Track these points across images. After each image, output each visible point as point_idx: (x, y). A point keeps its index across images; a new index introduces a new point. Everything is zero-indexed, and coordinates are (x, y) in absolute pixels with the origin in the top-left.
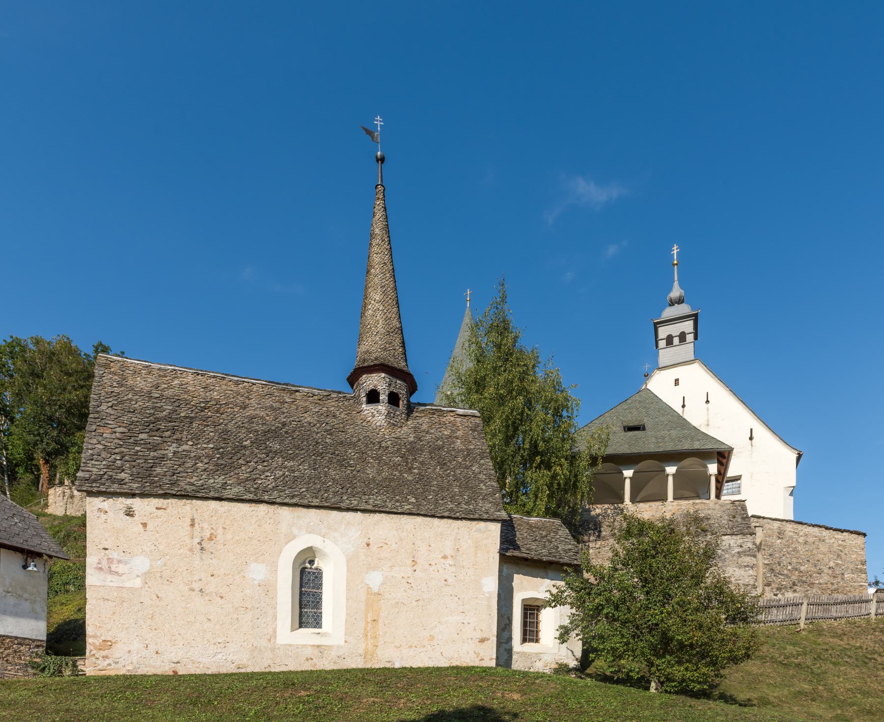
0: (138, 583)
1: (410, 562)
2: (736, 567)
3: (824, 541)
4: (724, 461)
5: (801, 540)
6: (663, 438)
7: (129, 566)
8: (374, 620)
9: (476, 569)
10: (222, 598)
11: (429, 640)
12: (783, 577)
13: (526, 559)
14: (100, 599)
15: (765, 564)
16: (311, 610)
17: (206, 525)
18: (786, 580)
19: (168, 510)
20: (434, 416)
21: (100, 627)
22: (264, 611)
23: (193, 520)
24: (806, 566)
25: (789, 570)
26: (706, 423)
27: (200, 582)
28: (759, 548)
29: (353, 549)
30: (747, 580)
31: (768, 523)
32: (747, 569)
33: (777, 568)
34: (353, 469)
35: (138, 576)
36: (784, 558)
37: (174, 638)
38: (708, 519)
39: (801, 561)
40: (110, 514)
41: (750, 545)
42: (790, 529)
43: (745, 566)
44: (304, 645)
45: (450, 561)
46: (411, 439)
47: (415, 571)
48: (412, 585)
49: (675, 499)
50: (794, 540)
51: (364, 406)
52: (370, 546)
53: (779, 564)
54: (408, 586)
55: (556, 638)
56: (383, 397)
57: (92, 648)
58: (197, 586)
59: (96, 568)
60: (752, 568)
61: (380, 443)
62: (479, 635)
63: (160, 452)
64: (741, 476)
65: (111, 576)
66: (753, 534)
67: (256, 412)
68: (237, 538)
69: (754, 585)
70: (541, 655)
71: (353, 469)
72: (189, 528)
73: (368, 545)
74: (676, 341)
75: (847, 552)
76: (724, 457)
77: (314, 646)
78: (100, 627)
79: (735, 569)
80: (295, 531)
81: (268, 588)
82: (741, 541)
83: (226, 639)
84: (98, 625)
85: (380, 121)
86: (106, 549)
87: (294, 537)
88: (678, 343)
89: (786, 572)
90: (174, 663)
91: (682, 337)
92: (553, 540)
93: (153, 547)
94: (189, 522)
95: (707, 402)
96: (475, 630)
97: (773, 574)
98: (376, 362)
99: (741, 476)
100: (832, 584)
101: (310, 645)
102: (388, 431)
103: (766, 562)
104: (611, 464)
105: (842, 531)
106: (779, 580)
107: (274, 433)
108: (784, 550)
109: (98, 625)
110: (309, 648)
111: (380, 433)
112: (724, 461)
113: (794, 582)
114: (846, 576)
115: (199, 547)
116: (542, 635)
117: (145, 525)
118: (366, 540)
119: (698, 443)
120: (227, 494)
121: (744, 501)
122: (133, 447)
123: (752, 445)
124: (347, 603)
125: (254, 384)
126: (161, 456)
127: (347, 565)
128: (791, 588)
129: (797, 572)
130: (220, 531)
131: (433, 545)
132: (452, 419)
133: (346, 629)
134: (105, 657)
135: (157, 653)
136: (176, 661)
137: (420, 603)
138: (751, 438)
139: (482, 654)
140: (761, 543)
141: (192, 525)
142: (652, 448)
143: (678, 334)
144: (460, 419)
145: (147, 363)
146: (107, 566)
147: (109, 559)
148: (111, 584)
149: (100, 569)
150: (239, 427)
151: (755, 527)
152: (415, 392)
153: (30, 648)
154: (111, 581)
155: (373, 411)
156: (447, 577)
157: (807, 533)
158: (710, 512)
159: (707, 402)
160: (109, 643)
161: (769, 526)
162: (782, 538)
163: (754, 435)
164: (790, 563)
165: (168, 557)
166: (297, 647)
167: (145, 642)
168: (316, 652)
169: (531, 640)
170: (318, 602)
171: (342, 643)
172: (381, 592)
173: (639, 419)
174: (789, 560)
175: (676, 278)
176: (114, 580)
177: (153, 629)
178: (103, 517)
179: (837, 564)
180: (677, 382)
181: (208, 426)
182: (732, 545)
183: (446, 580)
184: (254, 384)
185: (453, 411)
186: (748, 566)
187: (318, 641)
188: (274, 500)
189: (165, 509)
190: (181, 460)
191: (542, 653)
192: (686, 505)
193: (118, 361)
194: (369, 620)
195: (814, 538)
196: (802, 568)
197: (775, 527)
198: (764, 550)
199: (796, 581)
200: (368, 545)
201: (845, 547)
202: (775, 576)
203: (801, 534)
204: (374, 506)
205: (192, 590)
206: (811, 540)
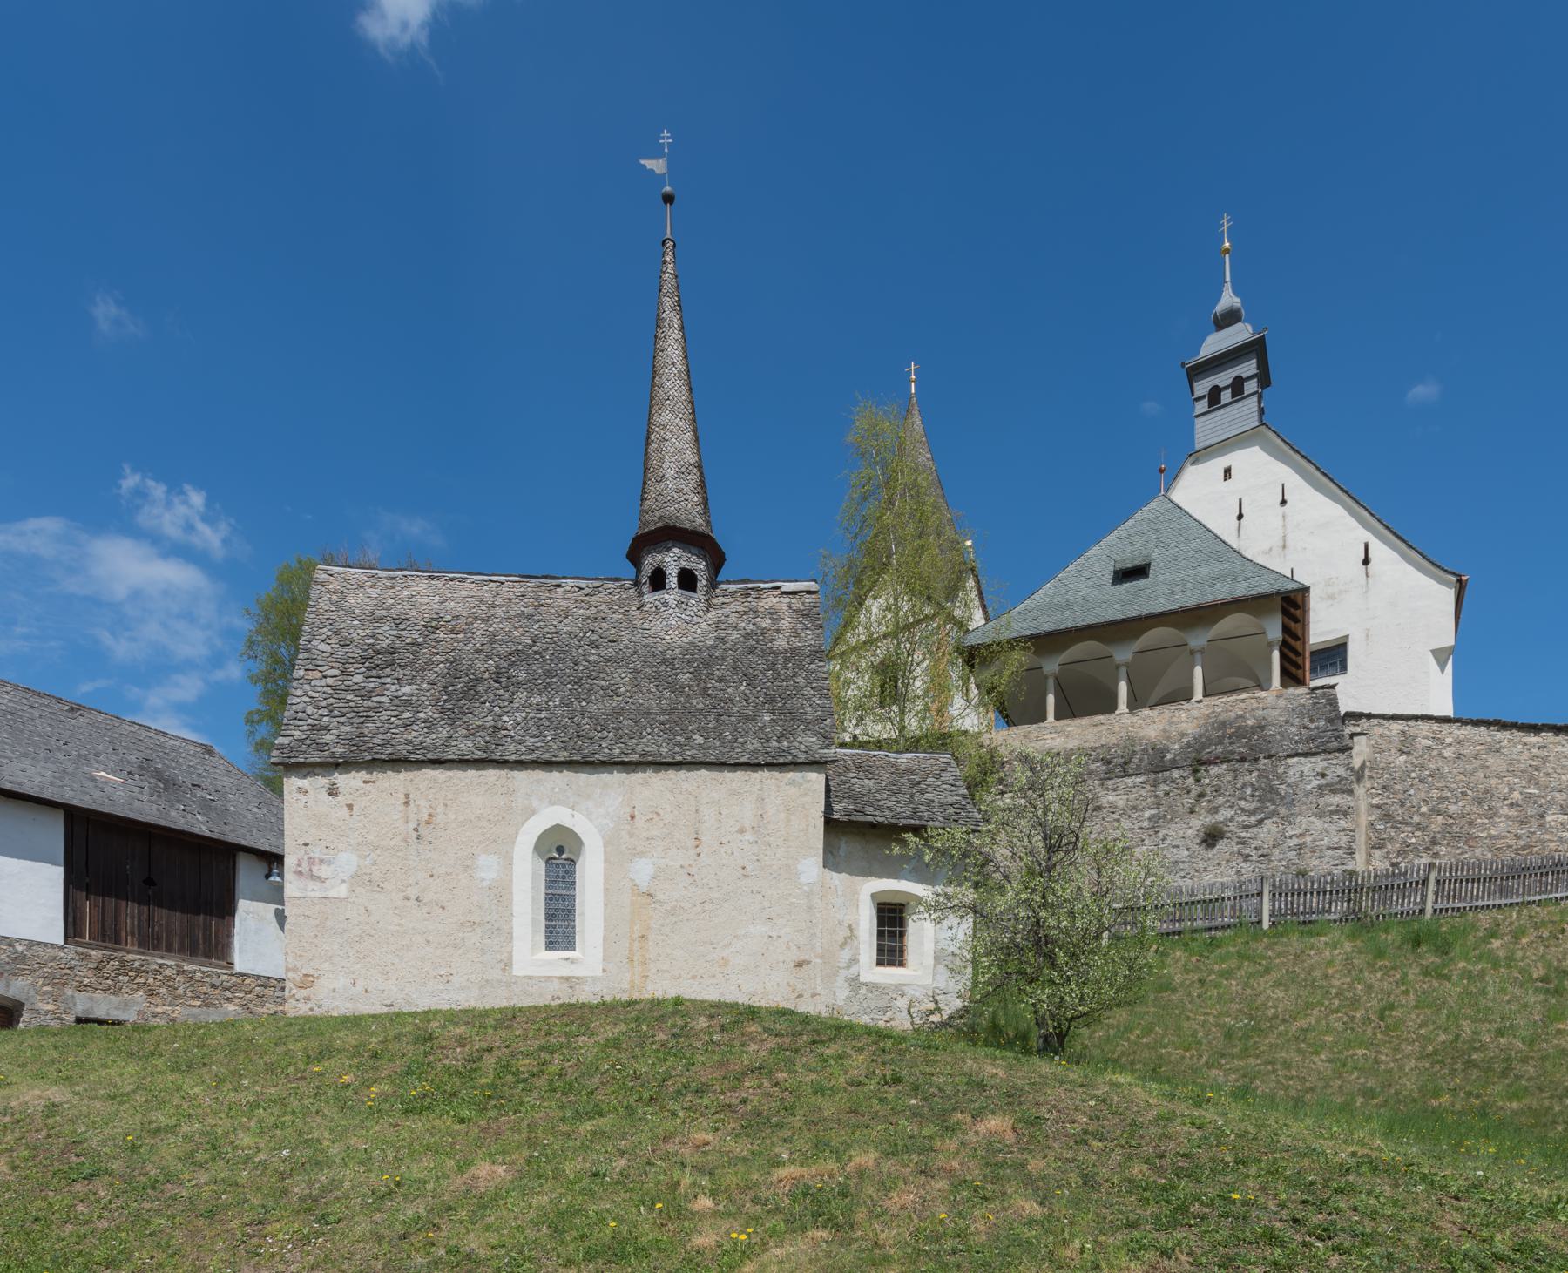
0: (342, 891)
1: (691, 842)
2: (1314, 815)
3: (1498, 751)
4: (1298, 613)
5: (1448, 753)
6: (1184, 583)
7: (333, 867)
8: (643, 937)
9: (789, 847)
10: (443, 908)
11: (720, 966)
12: (1409, 829)
13: (873, 826)
14: (299, 916)
15: (1372, 806)
16: (560, 923)
17: (422, 803)
18: (1417, 834)
19: (378, 784)
20: (749, 599)
21: (300, 956)
22: (496, 926)
23: (407, 796)
24: (1460, 804)
25: (1423, 814)
26: (1281, 543)
27: (417, 887)
28: (1359, 775)
29: (611, 826)
30: (1336, 839)
31: (1380, 725)
32: (1336, 817)
33: (1399, 813)
34: (621, 698)
35: (343, 881)
36: (1412, 792)
37: (387, 969)
38: (1262, 728)
39: (1449, 795)
40: (311, 792)
41: (1341, 771)
42: (1424, 733)
43: (1332, 813)
44: (549, 977)
45: (749, 837)
46: (710, 642)
47: (699, 854)
48: (696, 877)
49: (1205, 695)
50: (1435, 753)
51: (645, 597)
52: (636, 820)
53: (1402, 804)
54: (690, 879)
55: (281, 918)
56: (672, 581)
57: (292, 985)
58: (413, 892)
59: (295, 872)
60: (1345, 814)
61: (663, 653)
62: (795, 956)
63: (375, 699)
64: (1347, 636)
65: (312, 882)
66: (1347, 749)
67: (501, 626)
68: (461, 818)
69: (1350, 848)
70: (904, 988)
71: (621, 698)
72: (402, 808)
73: (633, 817)
74: (1226, 396)
75: (1550, 771)
76: (1297, 607)
77: (561, 978)
78: (300, 956)
79: (1312, 819)
80: (535, 803)
81: (501, 894)
82: (1324, 764)
83: (448, 969)
84: (299, 953)
85: (668, 138)
86: (306, 845)
87: (533, 812)
88: (1230, 400)
89: (1416, 819)
90: (386, 1006)
91: (1237, 386)
92: (930, 789)
93: (360, 839)
94: (402, 799)
95: (1284, 502)
96: (788, 947)
97: (1388, 825)
98: (660, 524)
99: (1347, 636)
100: (1518, 837)
101: (556, 977)
102: (677, 633)
103: (1375, 801)
104: (1097, 643)
105: (1535, 729)
106: (1402, 835)
107: (518, 656)
108: (1413, 775)
109: (299, 953)
110: (556, 981)
111: (667, 637)
112: (1298, 613)
113: (1434, 837)
114: (1548, 819)
115: (414, 834)
116: (910, 956)
117: (350, 807)
118: (629, 810)
119: (1244, 585)
120: (511, 751)
121: (1333, 687)
122: (343, 696)
123: (1367, 575)
124: (605, 910)
125: (502, 583)
126: (375, 705)
127: (605, 851)
128: (1428, 849)
129: (1440, 818)
130: (440, 809)
131: (724, 812)
132: (775, 600)
133: (605, 950)
134: (307, 999)
135: (366, 991)
136: (389, 1002)
137: (708, 906)
138: (1366, 562)
139: (800, 986)
140: (1363, 766)
141: (407, 803)
142: (1161, 605)
143: (1229, 382)
144: (787, 600)
145: (373, 571)
146: (308, 869)
147: (310, 858)
148: (313, 894)
149: (300, 873)
150: (478, 651)
151: (1352, 735)
152: (723, 564)
153: (275, 991)
154: (313, 890)
155: (657, 603)
156: (747, 863)
157: (1462, 737)
158: (1265, 713)
159: (1284, 502)
160: (311, 979)
161: (1381, 731)
162: (1409, 753)
163: (1371, 555)
164: (1424, 801)
165: (378, 852)
166: (540, 979)
167: (352, 976)
168: (565, 986)
169: (891, 964)
170: (570, 911)
171: (599, 973)
172: (652, 891)
173: (1146, 553)
174: (1423, 795)
175: (1228, 278)
176: (316, 888)
177: (361, 956)
178: (304, 799)
179: (1530, 796)
180: (1227, 473)
181: (438, 654)
182: (1306, 773)
183: (744, 868)
184: (502, 583)
185: (778, 588)
186: (1336, 812)
187: (566, 971)
188: (507, 758)
189: (374, 782)
190: (399, 709)
191: (905, 985)
192: (1222, 705)
193: (338, 573)
194: (635, 936)
195: (1478, 748)
196: (1453, 809)
197: (1395, 732)
198: (1371, 777)
199: (1439, 836)
200: (633, 817)
201: (1545, 760)
202: (1392, 827)
203: (1449, 740)
204: (641, 755)
205: (408, 899)
206: (1469, 750)
